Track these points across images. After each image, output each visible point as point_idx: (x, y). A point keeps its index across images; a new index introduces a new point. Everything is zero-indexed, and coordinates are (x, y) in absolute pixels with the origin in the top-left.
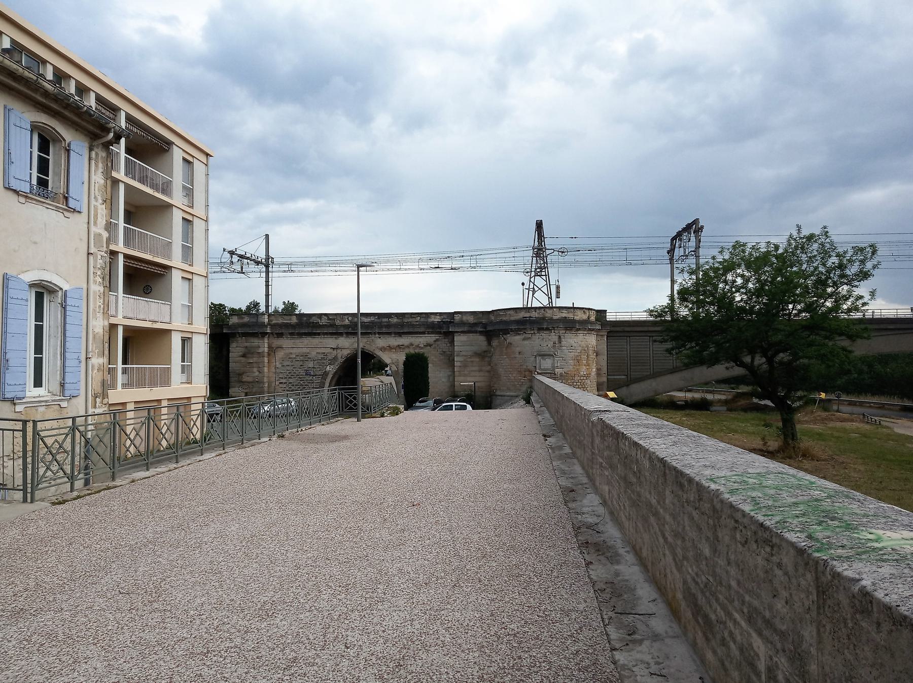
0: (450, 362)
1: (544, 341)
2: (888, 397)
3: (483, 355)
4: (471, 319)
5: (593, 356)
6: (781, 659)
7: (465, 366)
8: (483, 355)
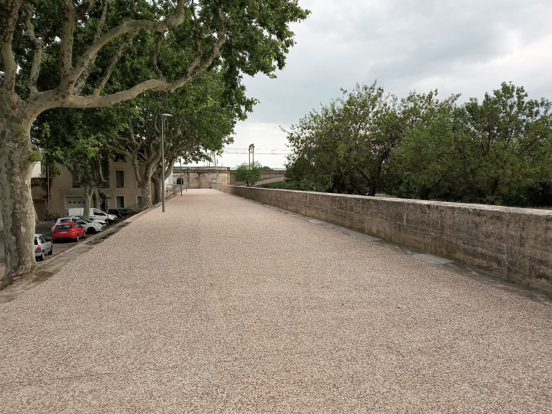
0: (188, 181)
1: (214, 175)
2: (492, 95)
3: (198, 179)
4: (194, 169)
5: (226, 179)
6: (361, 175)
7: (192, 181)
8: (198, 179)
